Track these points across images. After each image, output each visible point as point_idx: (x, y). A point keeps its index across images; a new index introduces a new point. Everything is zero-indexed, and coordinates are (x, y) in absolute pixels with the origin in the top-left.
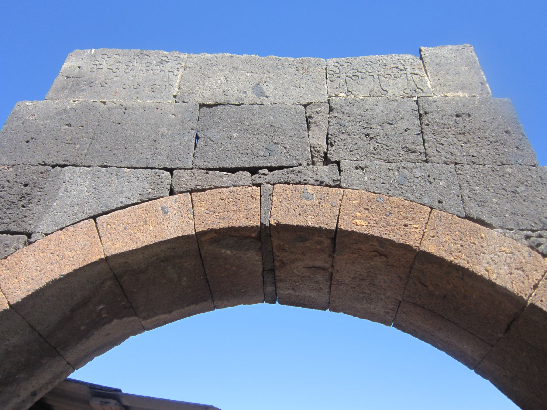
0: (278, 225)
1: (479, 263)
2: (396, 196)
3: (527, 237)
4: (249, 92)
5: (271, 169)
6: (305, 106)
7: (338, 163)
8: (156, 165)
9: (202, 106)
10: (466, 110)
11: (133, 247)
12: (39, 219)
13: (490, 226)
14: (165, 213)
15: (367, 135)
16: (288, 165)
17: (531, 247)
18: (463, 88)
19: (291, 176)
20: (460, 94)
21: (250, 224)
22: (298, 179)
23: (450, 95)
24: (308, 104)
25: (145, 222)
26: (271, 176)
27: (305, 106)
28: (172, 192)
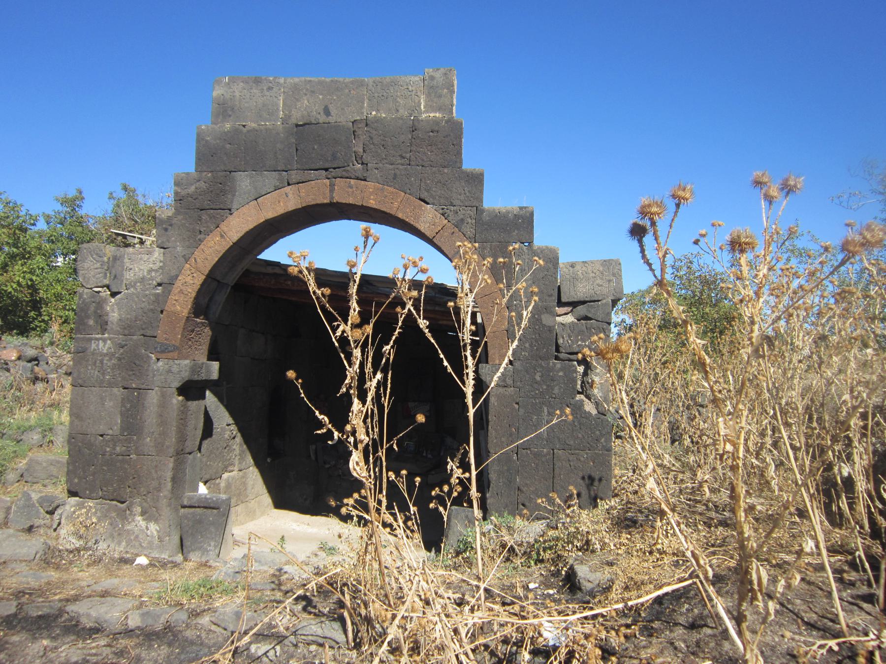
0: (337, 202)
1: (418, 222)
2: (390, 186)
3: (443, 209)
4: (322, 113)
5: (334, 168)
6: (353, 123)
7: (367, 164)
8: (279, 169)
9: (297, 126)
10: (436, 129)
11: (276, 215)
12: (232, 202)
13: (428, 203)
14: (287, 196)
15: (383, 146)
16: (343, 165)
17: (443, 215)
18: (439, 109)
19: (344, 173)
20: (437, 115)
21: (325, 201)
22: (347, 175)
23: (432, 115)
24: (355, 121)
25: (279, 202)
26: (334, 173)
27: (353, 123)
28: (289, 184)
